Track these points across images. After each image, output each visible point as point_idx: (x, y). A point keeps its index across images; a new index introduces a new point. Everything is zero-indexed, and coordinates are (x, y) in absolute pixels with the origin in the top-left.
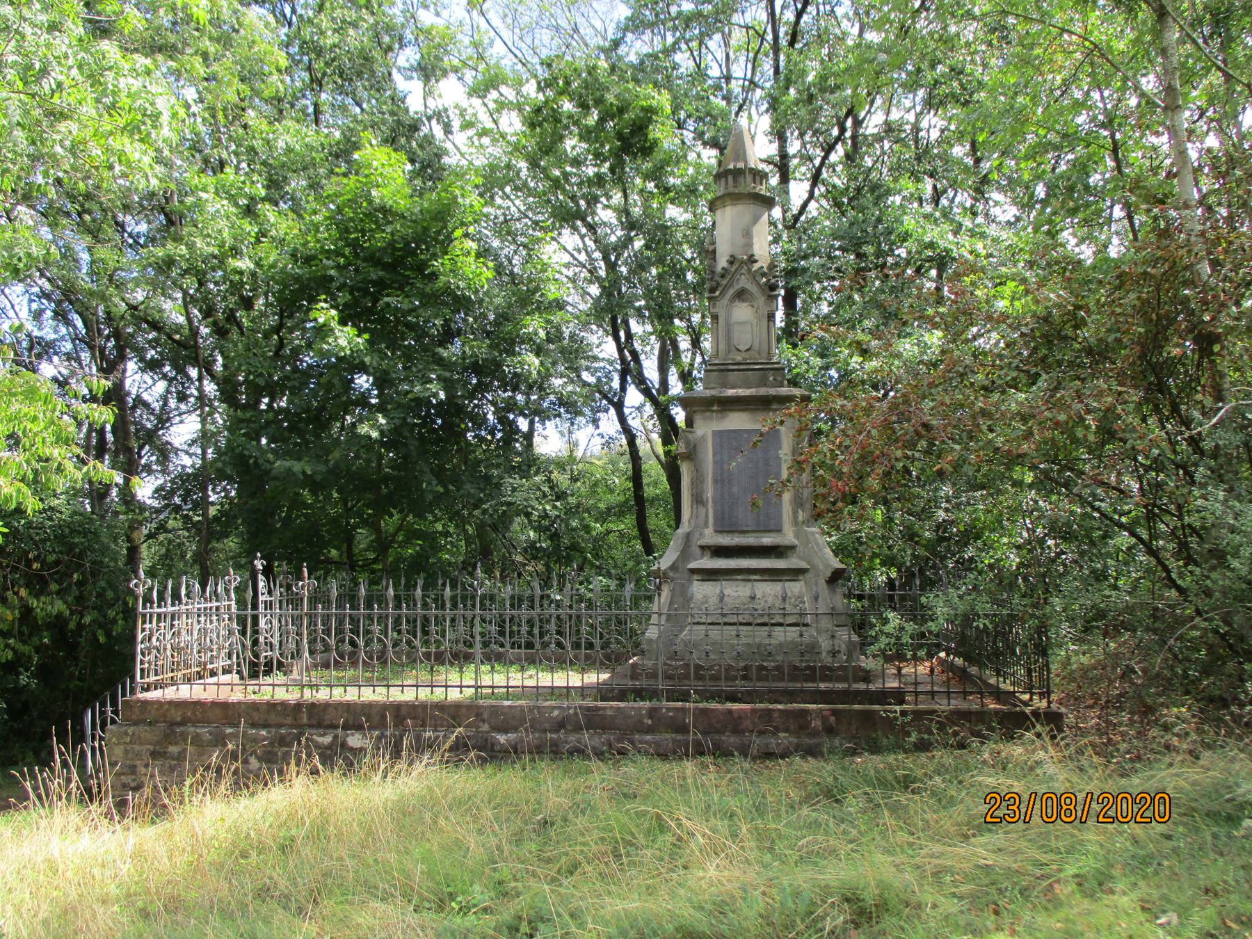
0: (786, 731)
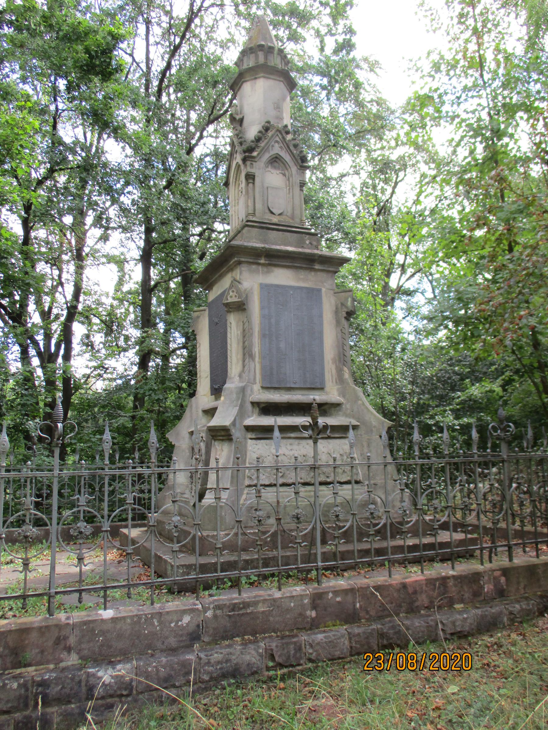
0: (462, 601)
